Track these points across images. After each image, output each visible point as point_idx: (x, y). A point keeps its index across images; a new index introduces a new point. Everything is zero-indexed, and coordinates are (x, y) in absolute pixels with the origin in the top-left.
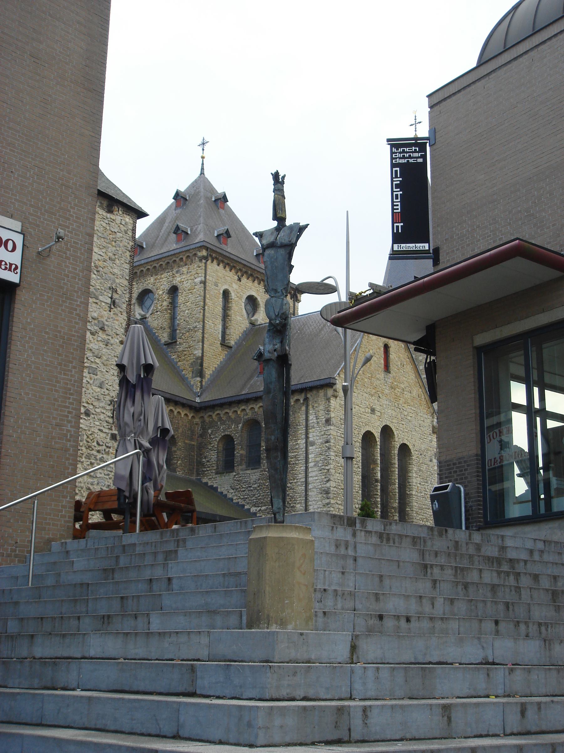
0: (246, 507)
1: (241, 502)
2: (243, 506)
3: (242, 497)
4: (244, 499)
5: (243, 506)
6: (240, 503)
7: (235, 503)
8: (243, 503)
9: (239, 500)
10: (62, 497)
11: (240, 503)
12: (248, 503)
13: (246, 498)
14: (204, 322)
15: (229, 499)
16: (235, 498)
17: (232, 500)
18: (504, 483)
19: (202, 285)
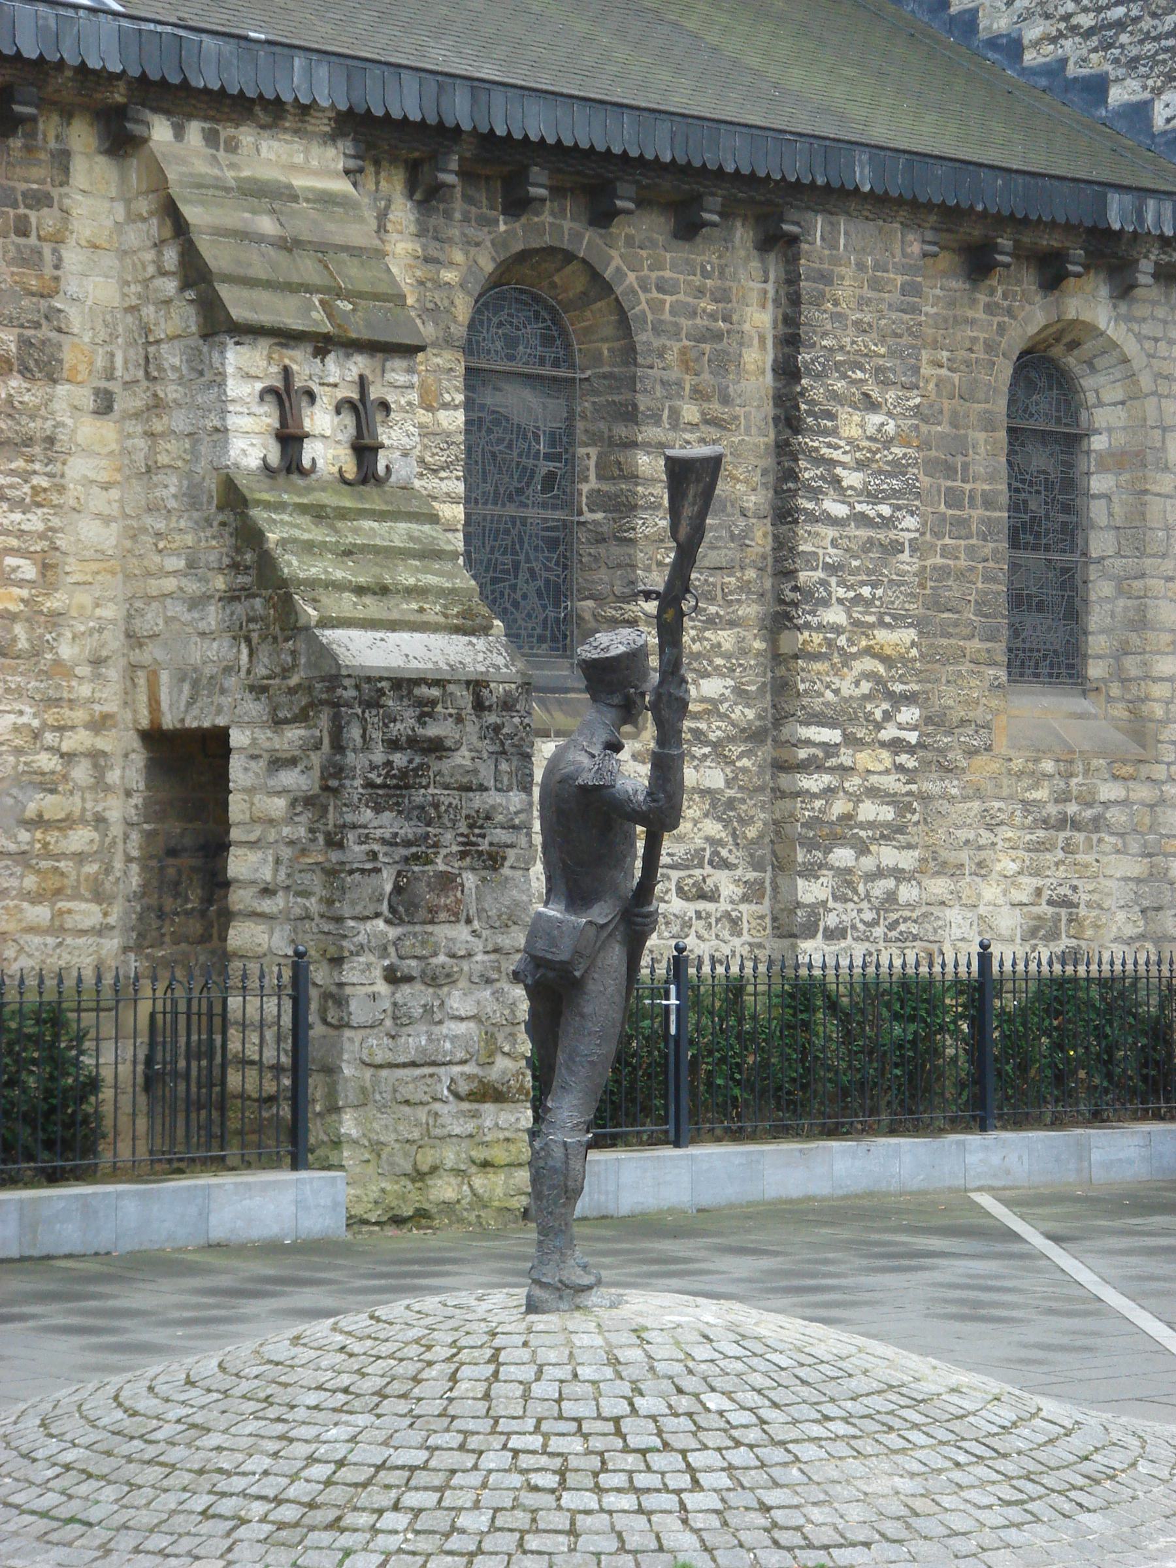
0: (1117, 95)
1: (1081, 58)
2: (1097, 87)
3: (1086, 21)
4: (1103, 34)
5: (1097, 87)
6: (1072, 71)
7: (1033, 72)
8: (1098, 63)
9: (1068, 45)
10: (660, 289)
11: (1072, 71)
12: (1133, 63)
13: (1120, 25)
14: (381, 1066)
15: (993, 43)
16: (1033, 32)
17: (1013, 47)
18: (102, 160)
19: (348, 419)
